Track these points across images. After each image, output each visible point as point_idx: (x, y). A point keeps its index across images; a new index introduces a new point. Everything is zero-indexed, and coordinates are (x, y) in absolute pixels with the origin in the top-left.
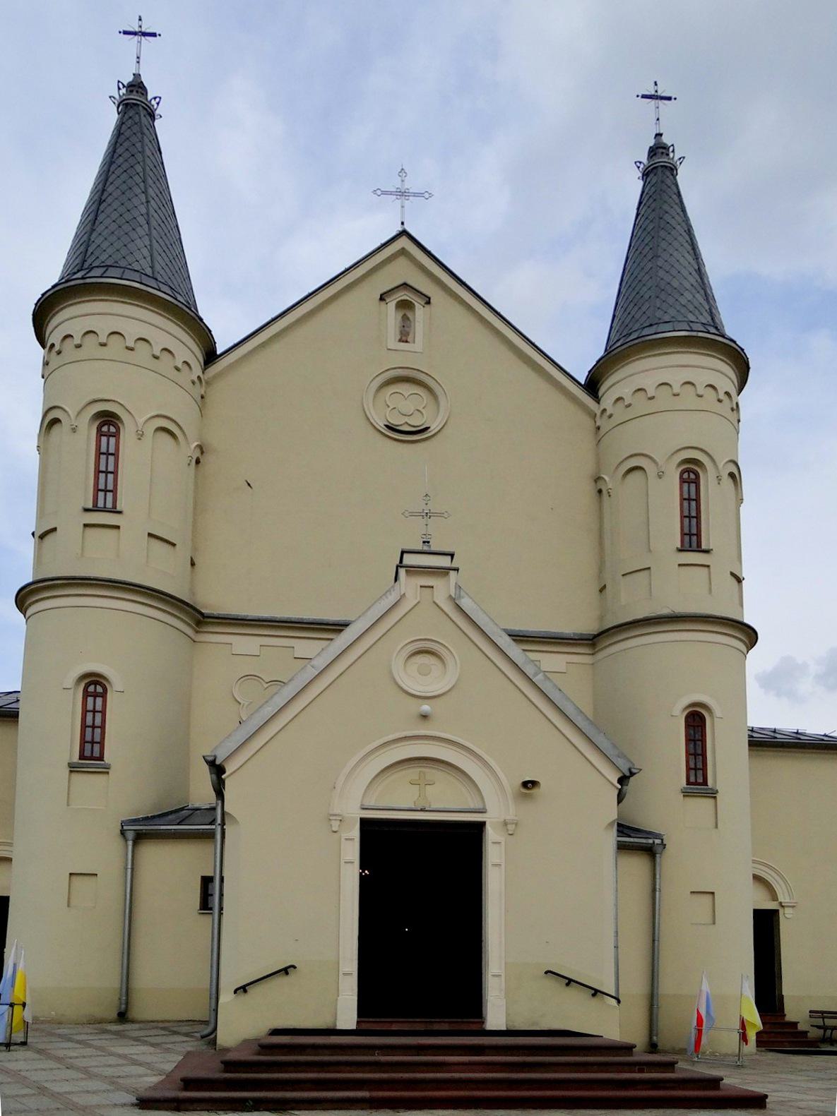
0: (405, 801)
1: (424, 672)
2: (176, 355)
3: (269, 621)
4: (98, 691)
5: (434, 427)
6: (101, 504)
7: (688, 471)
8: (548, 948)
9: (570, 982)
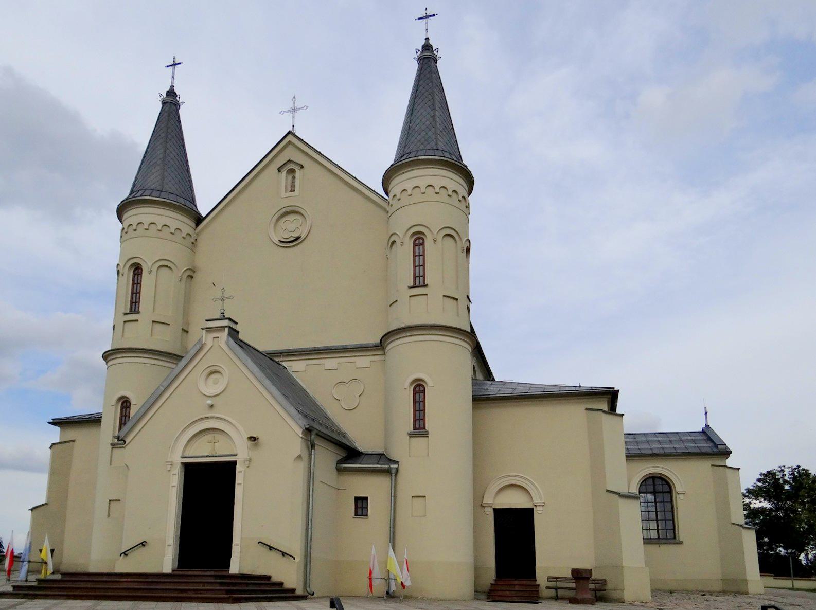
0: (203, 452)
1: (216, 383)
2: (170, 226)
3: (318, 350)
4: (421, 390)
5: (303, 236)
6: (417, 284)
7: (418, 238)
8: (261, 529)
9: (271, 548)
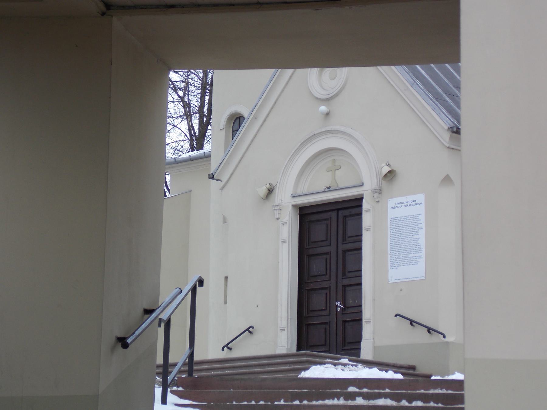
0: (320, 189)
9: (412, 322)
